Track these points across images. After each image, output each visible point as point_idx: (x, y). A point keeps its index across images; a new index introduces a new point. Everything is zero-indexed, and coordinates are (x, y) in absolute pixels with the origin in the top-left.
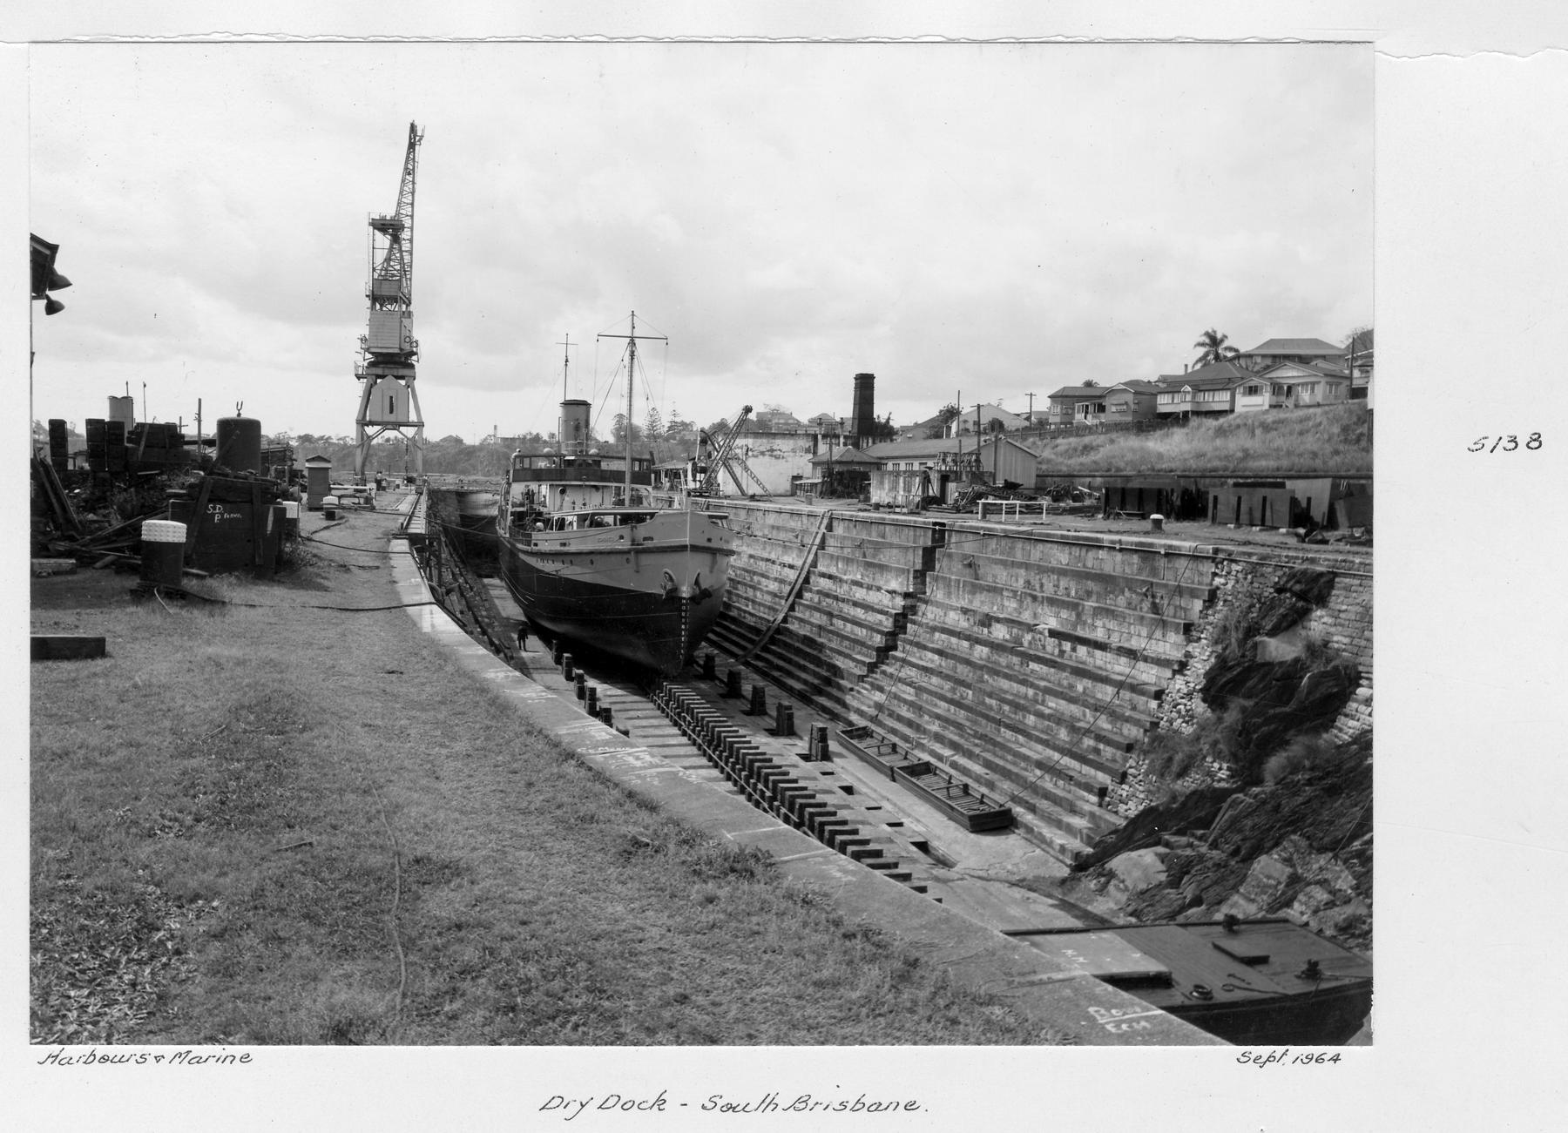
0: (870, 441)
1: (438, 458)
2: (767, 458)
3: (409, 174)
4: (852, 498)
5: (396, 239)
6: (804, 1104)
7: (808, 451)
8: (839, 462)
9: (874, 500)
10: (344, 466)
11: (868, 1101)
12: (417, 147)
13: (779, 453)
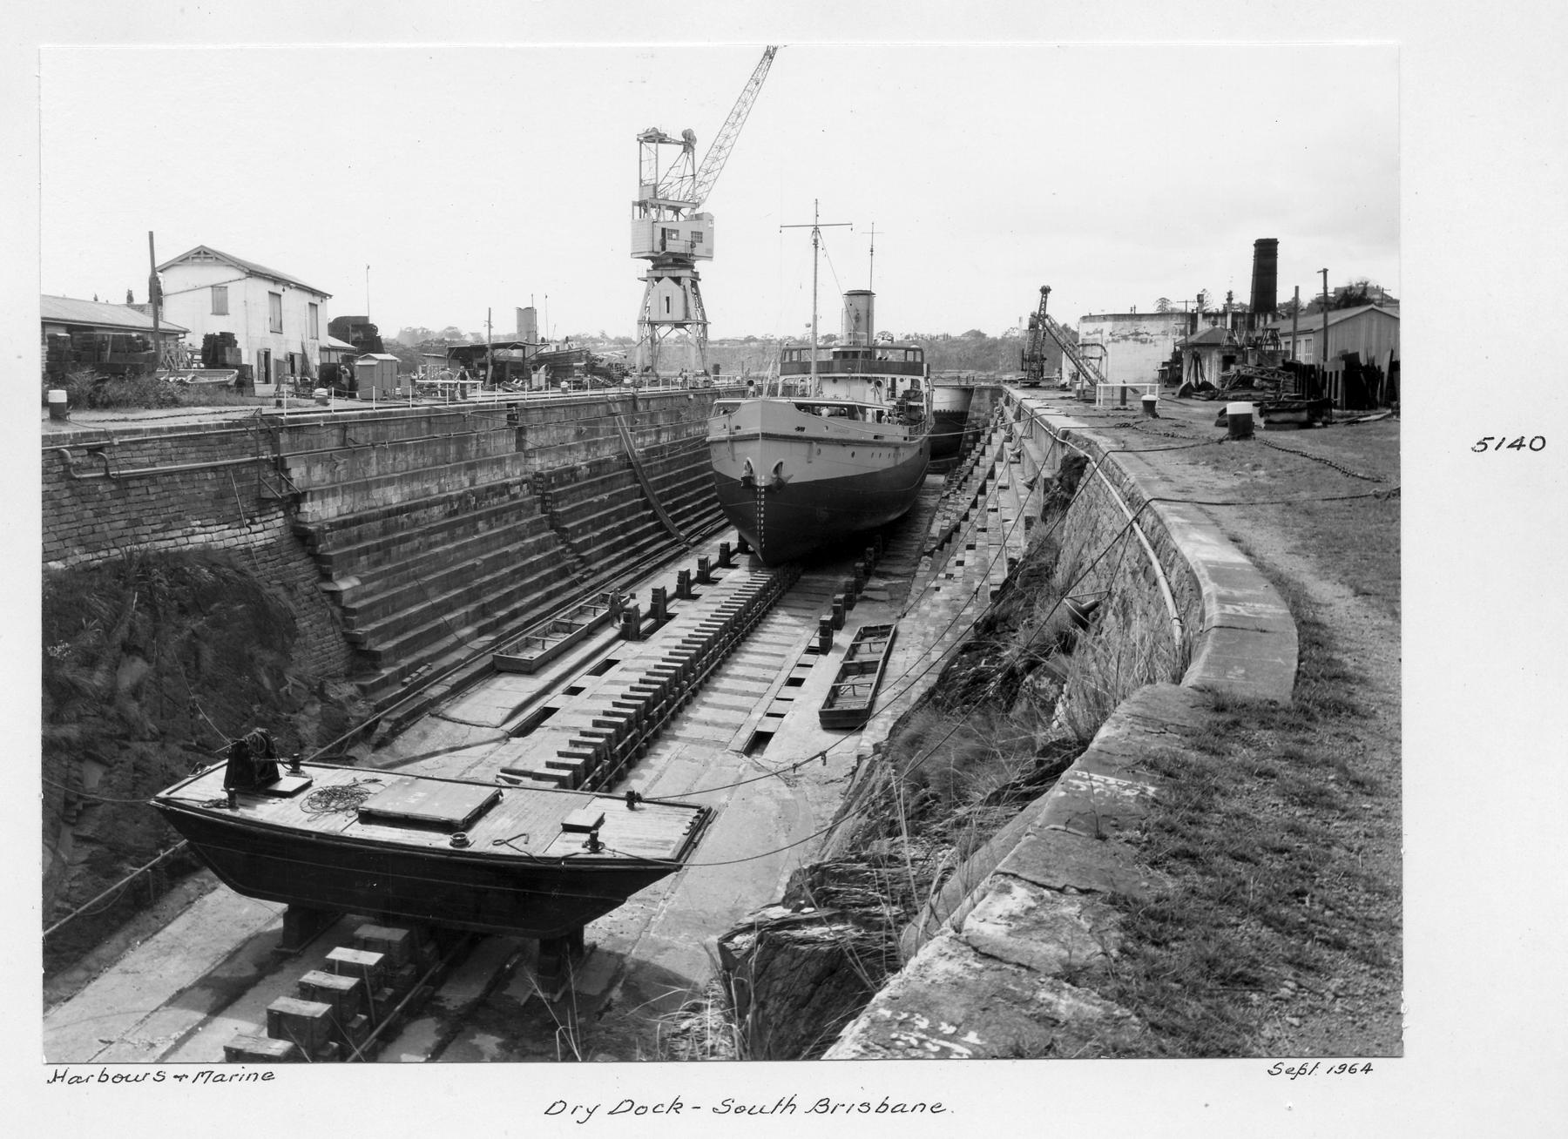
2: (1131, 343)
9: (535, 384)
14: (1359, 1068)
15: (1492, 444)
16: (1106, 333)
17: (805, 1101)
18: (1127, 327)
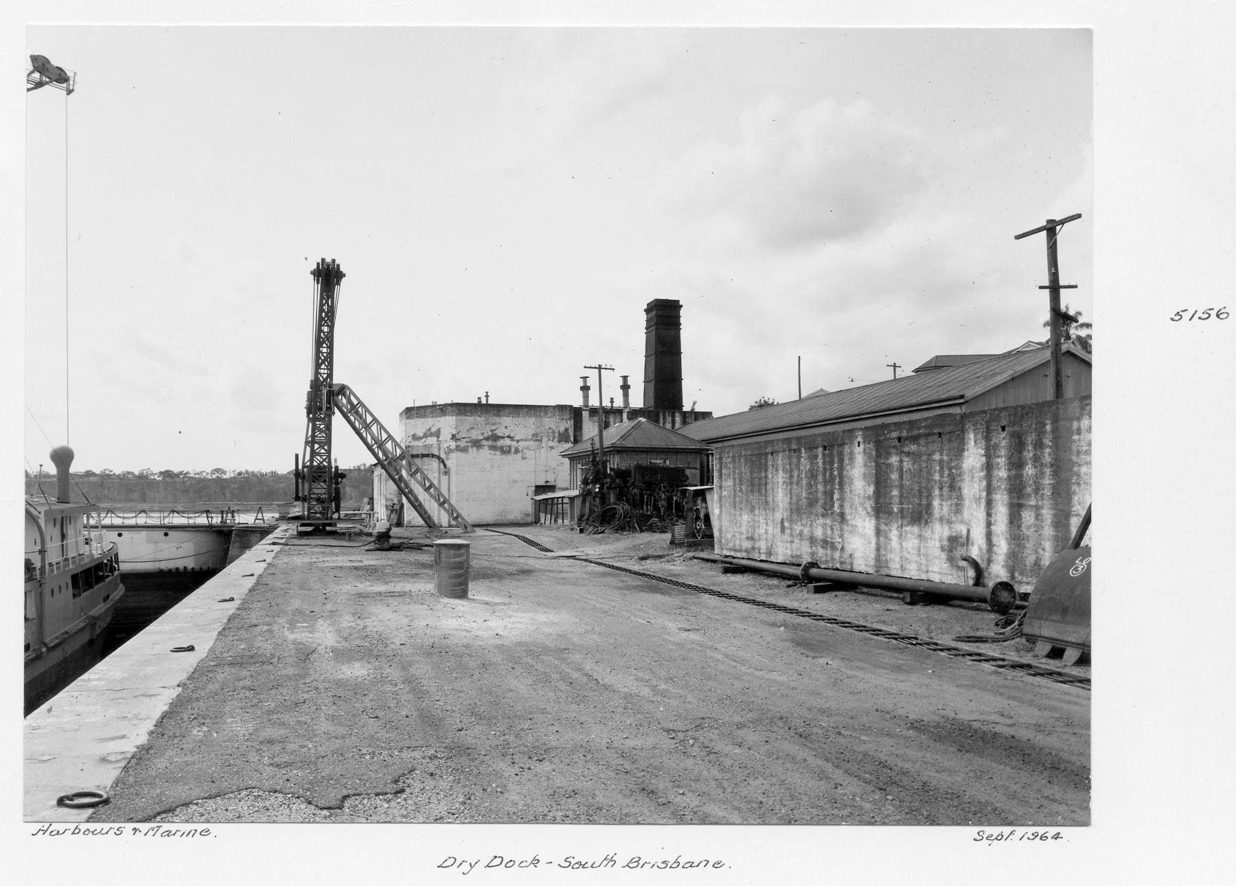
0: (678, 419)
1: (284, 488)
2: (485, 453)
4: (651, 529)
6: (636, 864)
7: (563, 437)
8: (618, 450)
10: (200, 497)
11: (682, 861)
13: (507, 442)
14: (1049, 835)
15: (1186, 316)
16: (446, 435)
17: (622, 860)
18: (478, 426)
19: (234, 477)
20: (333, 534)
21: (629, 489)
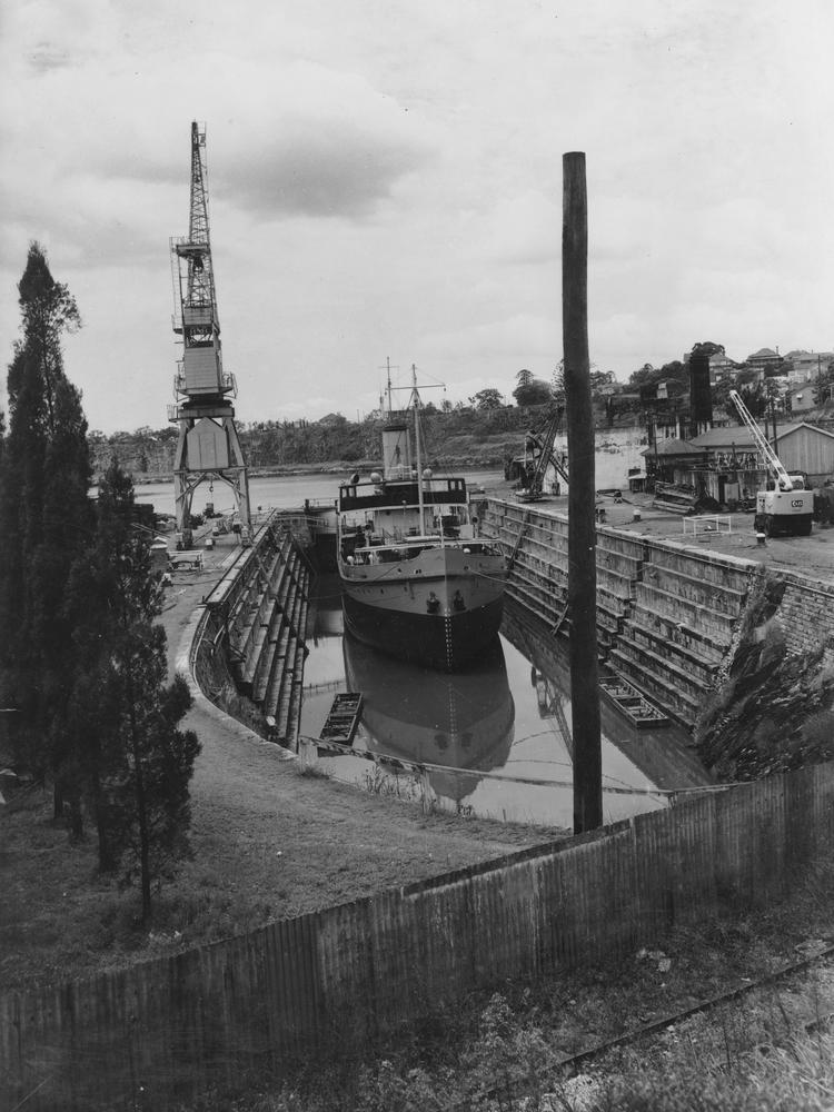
0: (708, 426)
3: (197, 181)
5: (198, 263)
7: (643, 442)
8: (665, 456)
12: (201, 149)
19: (255, 431)
20: (538, 502)
21: (670, 750)
